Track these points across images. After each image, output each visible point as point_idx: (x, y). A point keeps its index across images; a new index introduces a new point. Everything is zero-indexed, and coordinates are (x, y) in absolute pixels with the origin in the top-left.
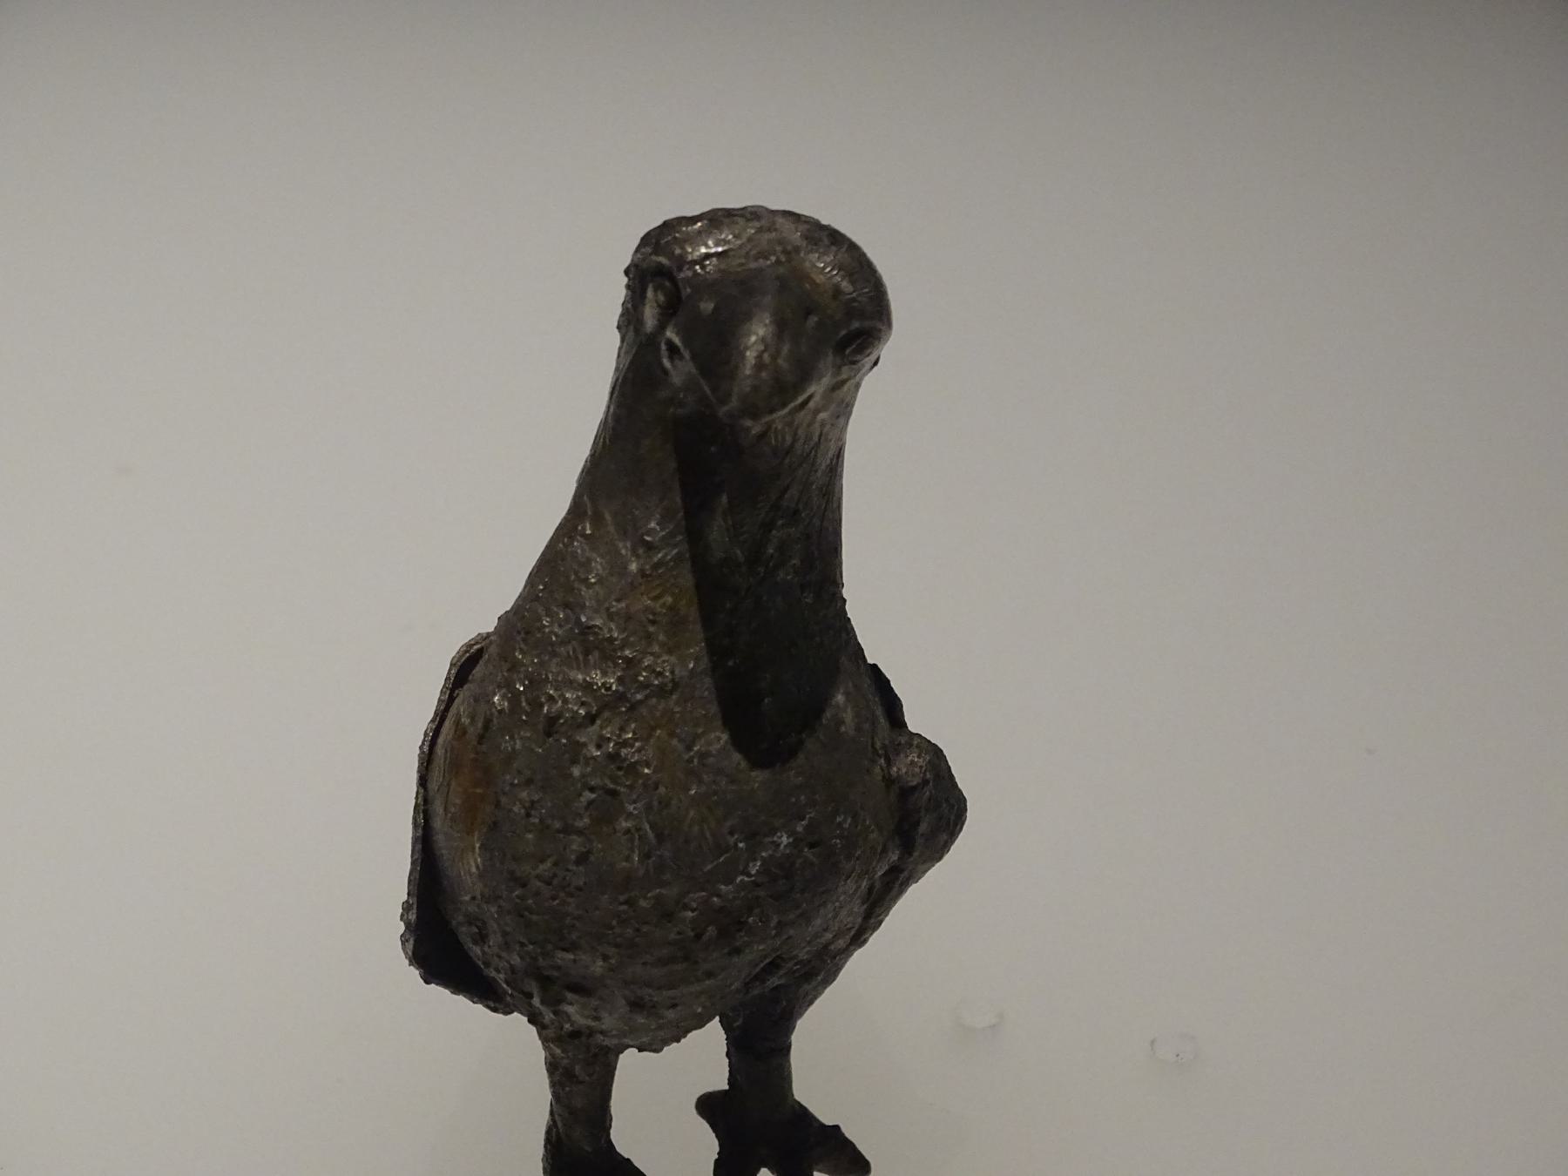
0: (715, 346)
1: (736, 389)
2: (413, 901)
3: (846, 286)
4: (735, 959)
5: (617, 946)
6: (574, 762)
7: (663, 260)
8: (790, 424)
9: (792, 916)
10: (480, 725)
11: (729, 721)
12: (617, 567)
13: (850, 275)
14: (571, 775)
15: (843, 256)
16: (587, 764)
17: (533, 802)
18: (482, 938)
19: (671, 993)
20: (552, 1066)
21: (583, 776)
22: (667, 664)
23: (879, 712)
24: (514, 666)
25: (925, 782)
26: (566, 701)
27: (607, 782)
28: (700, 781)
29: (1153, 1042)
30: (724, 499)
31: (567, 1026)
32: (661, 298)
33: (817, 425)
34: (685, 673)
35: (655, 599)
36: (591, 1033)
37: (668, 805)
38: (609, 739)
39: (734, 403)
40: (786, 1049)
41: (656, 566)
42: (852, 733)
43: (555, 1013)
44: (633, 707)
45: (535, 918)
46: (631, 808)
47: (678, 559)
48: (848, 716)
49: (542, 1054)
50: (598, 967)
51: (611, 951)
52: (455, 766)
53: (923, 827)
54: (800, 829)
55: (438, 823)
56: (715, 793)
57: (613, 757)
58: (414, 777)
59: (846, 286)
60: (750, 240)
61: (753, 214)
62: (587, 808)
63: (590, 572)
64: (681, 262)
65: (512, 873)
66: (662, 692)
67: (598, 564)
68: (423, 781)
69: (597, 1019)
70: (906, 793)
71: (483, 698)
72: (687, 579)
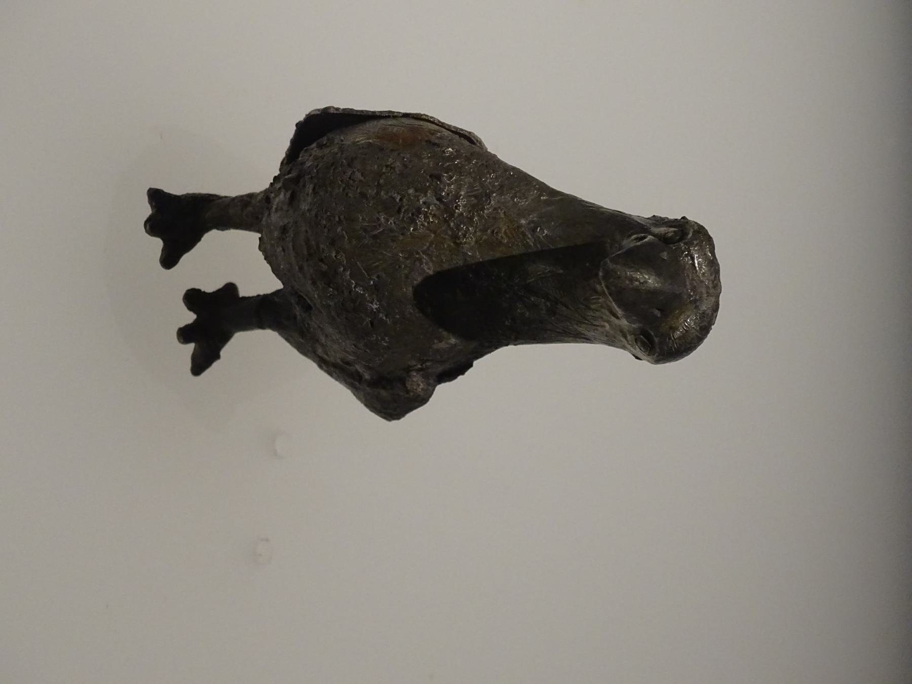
0: (642, 257)
1: (619, 267)
2: (341, 112)
3: (678, 334)
4: (309, 282)
5: (316, 216)
6: (416, 191)
7: (690, 235)
8: (602, 307)
9: (333, 313)
10: (437, 141)
11: (439, 275)
12: (522, 214)
13: (683, 337)
14: (409, 188)
15: (694, 333)
16: (415, 196)
17: (394, 168)
18: (321, 146)
19: (291, 247)
20: (251, 196)
21: (409, 195)
22: (471, 240)
23: (447, 366)
24: (468, 160)
25: (408, 392)
26: (449, 185)
27: (406, 207)
28: (406, 258)
29: (267, 540)
30: (561, 271)
31: (273, 195)
32: (670, 235)
33: (602, 323)
34: (465, 250)
35: (505, 233)
36: (269, 209)
37: (393, 241)
38: (428, 208)
39: (611, 266)
40: (262, 326)
41: (524, 235)
42: (435, 347)
43: (280, 189)
44: (446, 221)
45: (332, 171)
46: (391, 221)
47: (527, 246)
48: (443, 345)
49: (258, 191)
50: (304, 207)
51: (313, 213)
52: (413, 130)
53: (384, 393)
54: (381, 315)
55: (382, 122)
56: (400, 267)
57: (419, 211)
58: (408, 112)
59: (678, 334)
60: (702, 282)
61: (716, 285)
62: (391, 197)
63: (520, 198)
64: (689, 244)
65: (356, 158)
66: (455, 237)
67: (523, 203)
68: (406, 115)
69: (276, 209)
70: (402, 381)
71: (451, 144)
72: (515, 252)
